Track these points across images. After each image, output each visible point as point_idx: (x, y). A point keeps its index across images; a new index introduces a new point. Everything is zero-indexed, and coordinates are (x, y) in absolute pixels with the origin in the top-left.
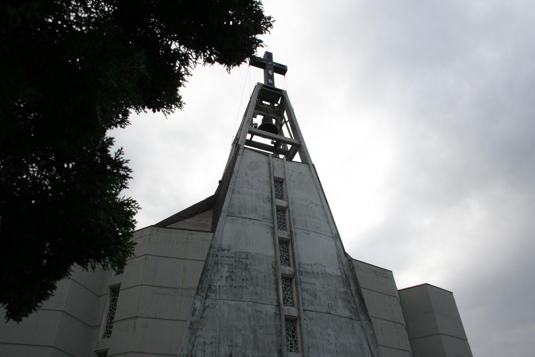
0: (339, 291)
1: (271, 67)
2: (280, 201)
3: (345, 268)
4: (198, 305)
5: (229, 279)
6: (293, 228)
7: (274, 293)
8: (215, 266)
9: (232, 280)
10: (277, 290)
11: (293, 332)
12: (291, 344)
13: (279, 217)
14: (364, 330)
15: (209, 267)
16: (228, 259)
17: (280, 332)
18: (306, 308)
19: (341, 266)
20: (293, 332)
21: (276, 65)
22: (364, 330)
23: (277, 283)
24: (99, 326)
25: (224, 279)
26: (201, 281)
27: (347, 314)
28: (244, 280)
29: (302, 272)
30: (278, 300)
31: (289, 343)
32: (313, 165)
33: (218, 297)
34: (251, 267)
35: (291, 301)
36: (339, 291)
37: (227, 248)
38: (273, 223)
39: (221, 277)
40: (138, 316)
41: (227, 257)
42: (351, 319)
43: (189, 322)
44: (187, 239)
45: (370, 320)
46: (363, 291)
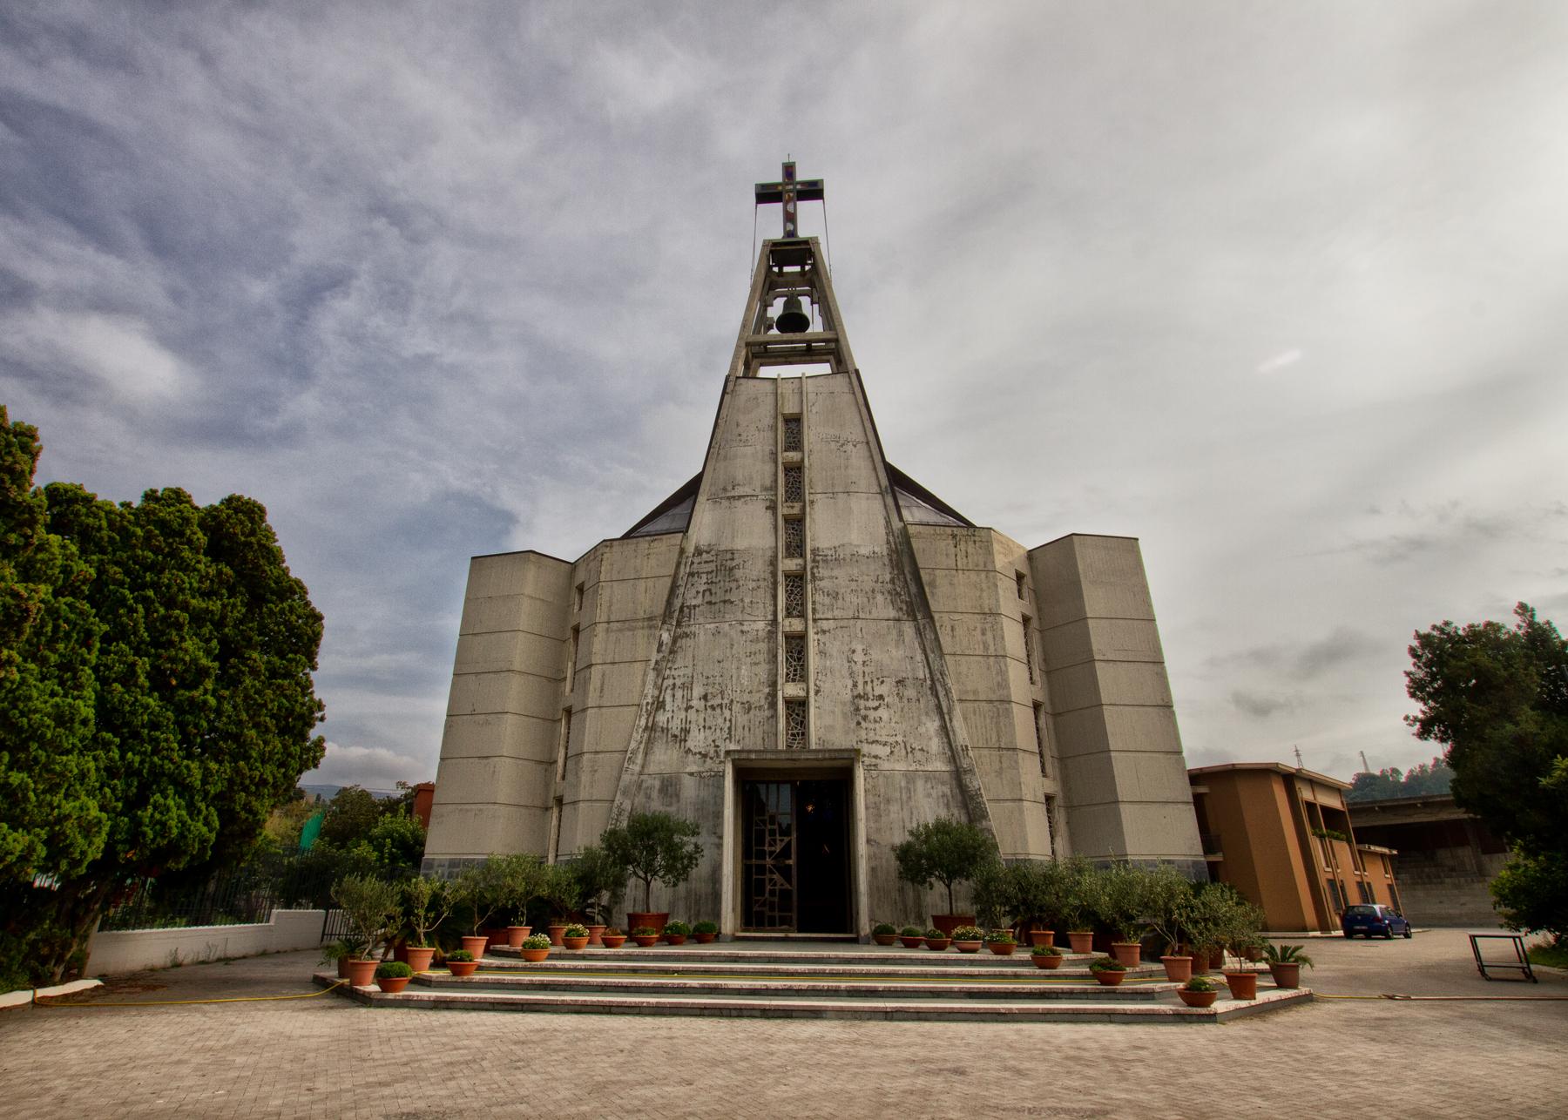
0: (880, 580)
1: (791, 195)
2: (482, 948)
3: (897, 541)
4: (666, 637)
5: (707, 593)
6: (807, 492)
7: (769, 601)
8: (690, 578)
9: (711, 594)
10: (775, 597)
11: (799, 653)
12: (795, 670)
13: (791, 479)
14: (920, 634)
15: (680, 582)
16: (706, 565)
17: (775, 656)
18: (818, 616)
19: (891, 539)
20: (799, 653)
21: (805, 188)
22: (920, 634)
23: (775, 583)
24: (565, 679)
25: (700, 595)
26: (669, 603)
27: (892, 613)
28: (726, 591)
29: (818, 562)
30: (775, 613)
31: (792, 669)
32: (857, 372)
33: (692, 622)
34: (832, 432)
35: (799, 608)
36: (880, 580)
37: (705, 548)
38: (776, 495)
39: (698, 592)
40: (564, 807)
41: (706, 562)
42: (898, 620)
43: (653, 661)
44: (600, 707)
45: (932, 618)
46: (922, 573)
